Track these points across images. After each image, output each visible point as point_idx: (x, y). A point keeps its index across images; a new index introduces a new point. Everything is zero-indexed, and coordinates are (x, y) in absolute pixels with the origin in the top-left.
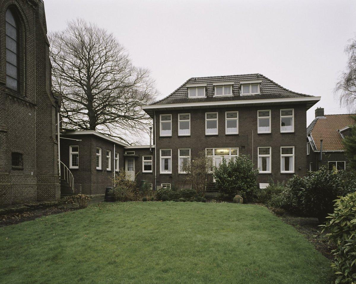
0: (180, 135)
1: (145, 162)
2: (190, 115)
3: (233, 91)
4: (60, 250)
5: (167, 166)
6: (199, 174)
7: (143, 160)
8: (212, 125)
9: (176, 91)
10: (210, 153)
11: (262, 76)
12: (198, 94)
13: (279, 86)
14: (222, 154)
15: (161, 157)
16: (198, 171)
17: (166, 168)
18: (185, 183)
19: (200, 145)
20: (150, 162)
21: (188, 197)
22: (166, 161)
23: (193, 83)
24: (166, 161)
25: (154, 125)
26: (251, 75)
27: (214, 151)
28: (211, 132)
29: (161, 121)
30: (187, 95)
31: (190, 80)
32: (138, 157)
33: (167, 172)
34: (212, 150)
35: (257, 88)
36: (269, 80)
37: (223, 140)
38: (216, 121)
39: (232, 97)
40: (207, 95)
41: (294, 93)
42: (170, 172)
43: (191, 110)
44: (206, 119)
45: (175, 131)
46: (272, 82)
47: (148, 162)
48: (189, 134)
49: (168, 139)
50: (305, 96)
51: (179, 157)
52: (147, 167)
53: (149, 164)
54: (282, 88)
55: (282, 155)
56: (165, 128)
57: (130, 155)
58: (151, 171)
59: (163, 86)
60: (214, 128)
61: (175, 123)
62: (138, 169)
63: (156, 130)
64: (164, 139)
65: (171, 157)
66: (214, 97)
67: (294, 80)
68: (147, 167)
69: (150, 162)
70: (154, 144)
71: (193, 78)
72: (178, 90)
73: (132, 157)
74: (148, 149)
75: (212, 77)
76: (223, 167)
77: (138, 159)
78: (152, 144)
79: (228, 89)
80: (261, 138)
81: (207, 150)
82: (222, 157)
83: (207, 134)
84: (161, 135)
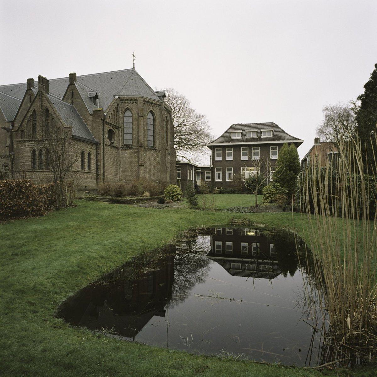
0: (227, 160)
1: (207, 175)
2: (259, 148)
3: (257, 134)
4: (191, 217)
5: (220, 177)
6: (238, 182)
7: (206, 174)
8: (245, 154)
9: (224, 134)
10: (244, 170)
11: (275, 124)
12: (268, 134)
13: (284, 131)
14: (251, 170)
15: (216, 172)
16: (238, 181)
17: (219, 178)
18: (229, 186)
19: (238, 165)
20: (210, 175)
21: (233, 192)
22: (219, 174)
23: (233, 127)
24: (219, 174)
25: (212, 154)
26: (269, 123)
27: (246, 169)
28: (244, 158)
29: (216, 152)
30: (231, 136)
31: (232, 126)
32: (203, 172)
33: (219, 181)
34: (245, 168)
35: (271, 133)
36: (279, 127)
37: (250, 163)
38: (221, 153)
39: (241, 139)
40: (242, 136)
41: (291, 136)
42: (221, 181)
43: (236, 145)
44: (242, 151)
45: (224, 158)
46: (280, 128)
47: (208, 175)
48: (232, 160)
49: (220, 162)
50: (296, 139)
51: (226, 172)
52: (208, 178)
53: (209, 176)
54: (285, 132)
55: (271, 171)
56: (219, 155)
57: (201, 171)
58: (210, 180)
59: (216, 130)
60: (275, 155)
61: (224, 153)
62: (203, 179)
63: (213, 157)
64: (218, 162)
65: (222, 172)
66: (246, 138)
67: (291, 128)
68: (208, 178)
69: (210, 175)
70: (212, 165)
71: (234, 125)
72: (225, 132)
73: (200, 172)
74: (209, 168)
75: (245, 124)
76: (250, 179)
77: (203, 173)
78: (211, 165)
79: (254, 134)
80: (272, 162)
81: (242, 168)
82: (249, 173)
83: (242, 159)
84: (216, 160)
